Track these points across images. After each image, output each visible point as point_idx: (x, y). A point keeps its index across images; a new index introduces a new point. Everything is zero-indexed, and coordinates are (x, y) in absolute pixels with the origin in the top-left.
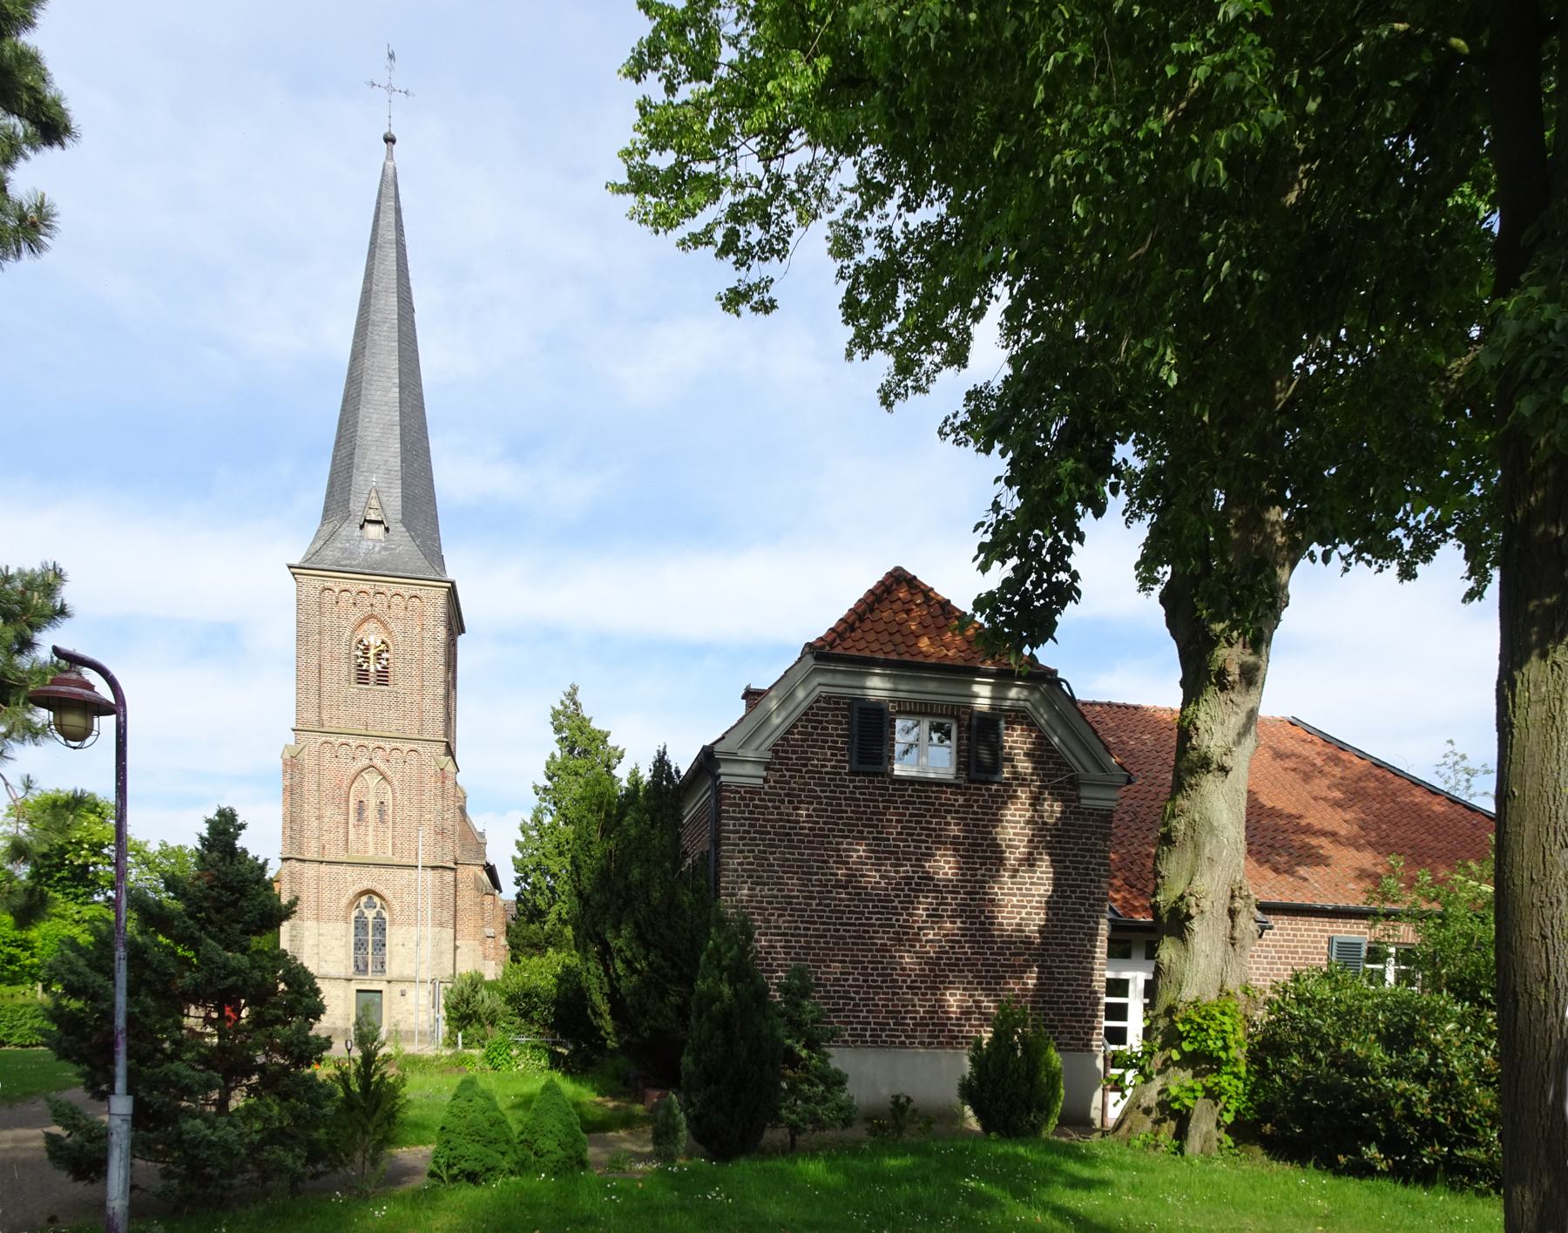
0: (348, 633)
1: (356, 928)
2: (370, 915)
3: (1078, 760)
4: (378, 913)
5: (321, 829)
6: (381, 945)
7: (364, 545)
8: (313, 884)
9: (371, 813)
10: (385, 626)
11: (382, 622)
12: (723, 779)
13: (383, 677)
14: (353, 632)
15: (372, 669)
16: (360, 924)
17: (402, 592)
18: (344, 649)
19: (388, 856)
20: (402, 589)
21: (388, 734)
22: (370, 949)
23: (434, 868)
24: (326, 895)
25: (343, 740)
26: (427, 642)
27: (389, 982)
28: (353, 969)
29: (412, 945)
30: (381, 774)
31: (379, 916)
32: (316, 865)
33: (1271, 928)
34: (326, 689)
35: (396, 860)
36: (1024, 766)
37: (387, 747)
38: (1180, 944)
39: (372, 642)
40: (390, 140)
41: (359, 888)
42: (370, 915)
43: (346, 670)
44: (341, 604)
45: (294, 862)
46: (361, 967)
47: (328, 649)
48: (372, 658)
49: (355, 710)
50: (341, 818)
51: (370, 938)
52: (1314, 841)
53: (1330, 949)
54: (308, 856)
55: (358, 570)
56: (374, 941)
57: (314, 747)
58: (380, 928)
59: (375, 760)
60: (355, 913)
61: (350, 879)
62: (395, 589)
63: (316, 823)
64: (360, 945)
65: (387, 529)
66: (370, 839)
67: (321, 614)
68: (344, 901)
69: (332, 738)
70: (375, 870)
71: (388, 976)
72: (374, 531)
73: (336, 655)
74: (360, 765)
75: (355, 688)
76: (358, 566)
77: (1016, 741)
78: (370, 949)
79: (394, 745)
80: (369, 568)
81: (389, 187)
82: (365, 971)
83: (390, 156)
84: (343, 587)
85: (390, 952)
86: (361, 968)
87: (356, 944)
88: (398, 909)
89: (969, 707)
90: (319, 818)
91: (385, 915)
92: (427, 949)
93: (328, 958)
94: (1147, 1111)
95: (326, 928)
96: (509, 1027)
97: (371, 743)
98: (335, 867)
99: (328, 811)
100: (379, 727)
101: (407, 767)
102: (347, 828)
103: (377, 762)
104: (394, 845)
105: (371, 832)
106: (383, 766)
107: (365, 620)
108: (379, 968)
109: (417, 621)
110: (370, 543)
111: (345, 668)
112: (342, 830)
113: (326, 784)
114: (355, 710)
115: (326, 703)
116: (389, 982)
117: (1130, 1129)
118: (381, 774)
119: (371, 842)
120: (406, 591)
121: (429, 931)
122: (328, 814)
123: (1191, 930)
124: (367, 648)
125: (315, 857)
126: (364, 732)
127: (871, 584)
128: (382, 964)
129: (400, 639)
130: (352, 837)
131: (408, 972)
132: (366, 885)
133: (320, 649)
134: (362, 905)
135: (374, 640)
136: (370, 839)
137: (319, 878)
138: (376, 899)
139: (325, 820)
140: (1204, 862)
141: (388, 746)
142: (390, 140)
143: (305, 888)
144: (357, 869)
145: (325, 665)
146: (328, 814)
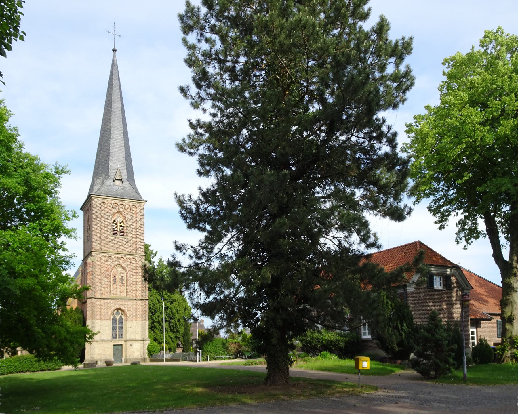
0: (110, 217)
1: (113, 322)
2: (118, 317)
3: (463, 284)
4: (121, 316)
5: (101, 287)
6: (121, 328)
7: (115, 187)
8: (99, 307)
9: (118, 281)
10: (123, 215)
11: (122, 214)
12: (408, 291)
13: (122, 233)
14: (112, 217)
15: (119, 230)
16: (114, 321)
17: (129, 204)
18: (109, 223)
19: (124, 295)
20: (129, 203)
21: (125, 253)
22: (118, 330)
23: (142, 300)
24: (103, 310)
25: (109, 255)
26: (138, 221)
27: (125, 341)
28: (111, 337)
29: (134, 327)
30: (122, 267)
31: (121, 317)
32: (100, 300)
33: (493, 319)
34: (103, 237)
35: (128, 297)
36: (455, 284)
37: (119, 257)
38: (510, 325)
39: (119, 221)
40: (114, 51)
41: (115, 307)
42: (118, 317)
43: (110, 231)
44: (108, 208)
45: (93, 299)
46: (114, 336)
47: (104, 223)
48: (119, 226)
49: (113, 244)
50: (108, 283)
51: (118, 326)
52: (482, 297)
53: (497, 322)
54: (97, 297)
55: (115, 196)
56: (119, 327)
57: (99, 258)
58: (121, 322)
59: (120, 262)
60: (112, 317)
61: (112, 305)
62: (127, 203)
63: (100, 285)
64: (114, 328)
65: (123, 182)
66: (118, 290)
67: (101, 211)
68: (110, 313)
69: (105, 255)
70: (120, 301)
71: (124, 339)
72: (118, 183)
73: (106, 225)
74: (115, 264)
75: (113, 237)
76: (114, 194)
77: (453, 279)
78: (118, 330)
79: (121, 256)
80: (118, 195)
81: (114, 64)
82: (116, 338)
83: (114, 56)
84: (109, 202)
85: (126, 331)
86: (114, 337)
87: (112, 328)
88: (129, 315)
89: (446, 273)
90: (101, 283)
91: (123, 317)
92: (139, 329)
93: (104, 334)
94: (509, 357)
95: (103, 322)
96: (223, 353)
97: (119, 256)
98: (106, 301)
99: (104, 280)
100: (121, 250)
101: (132, 264)
102: (110, 286)
103: (121, 263)
104: (127, 292)
105: (118, 288)
106: (123, 264)
107: (116, 213)
108: (121, 336)
109: (134, 214)
110: (117, 187)
111: (109, 230)
112: (109, 287)
113: (103, 271)
114: (113, 244)
115: (103, 242)
116: (125, 341)
117: (506, 361)
118: (122, 267)
119: (119, 291)
120: (131, 204)
121: (139, 322)
122: (104, 281)
123: (513, 322)
124: (117, 223)
125: (100, 297)
126: (117, 252)
127: (437, 252)
128: (122, 335)
129: (128, 220)
130: (112, 289)
131: (133, 337)
132: (118, 306)
133: (101, 223)
134: (115, 314)
135: (119, 220)
136: (118, 290)
137: (101, 305)
138: (120, 311)
139: (103, 284)
140: (514, 309)
141: (125, 257)
142: (114, 51)
143: (96, 308)
144: (114, 301)
145: (103, 229)
146: (104, 281)
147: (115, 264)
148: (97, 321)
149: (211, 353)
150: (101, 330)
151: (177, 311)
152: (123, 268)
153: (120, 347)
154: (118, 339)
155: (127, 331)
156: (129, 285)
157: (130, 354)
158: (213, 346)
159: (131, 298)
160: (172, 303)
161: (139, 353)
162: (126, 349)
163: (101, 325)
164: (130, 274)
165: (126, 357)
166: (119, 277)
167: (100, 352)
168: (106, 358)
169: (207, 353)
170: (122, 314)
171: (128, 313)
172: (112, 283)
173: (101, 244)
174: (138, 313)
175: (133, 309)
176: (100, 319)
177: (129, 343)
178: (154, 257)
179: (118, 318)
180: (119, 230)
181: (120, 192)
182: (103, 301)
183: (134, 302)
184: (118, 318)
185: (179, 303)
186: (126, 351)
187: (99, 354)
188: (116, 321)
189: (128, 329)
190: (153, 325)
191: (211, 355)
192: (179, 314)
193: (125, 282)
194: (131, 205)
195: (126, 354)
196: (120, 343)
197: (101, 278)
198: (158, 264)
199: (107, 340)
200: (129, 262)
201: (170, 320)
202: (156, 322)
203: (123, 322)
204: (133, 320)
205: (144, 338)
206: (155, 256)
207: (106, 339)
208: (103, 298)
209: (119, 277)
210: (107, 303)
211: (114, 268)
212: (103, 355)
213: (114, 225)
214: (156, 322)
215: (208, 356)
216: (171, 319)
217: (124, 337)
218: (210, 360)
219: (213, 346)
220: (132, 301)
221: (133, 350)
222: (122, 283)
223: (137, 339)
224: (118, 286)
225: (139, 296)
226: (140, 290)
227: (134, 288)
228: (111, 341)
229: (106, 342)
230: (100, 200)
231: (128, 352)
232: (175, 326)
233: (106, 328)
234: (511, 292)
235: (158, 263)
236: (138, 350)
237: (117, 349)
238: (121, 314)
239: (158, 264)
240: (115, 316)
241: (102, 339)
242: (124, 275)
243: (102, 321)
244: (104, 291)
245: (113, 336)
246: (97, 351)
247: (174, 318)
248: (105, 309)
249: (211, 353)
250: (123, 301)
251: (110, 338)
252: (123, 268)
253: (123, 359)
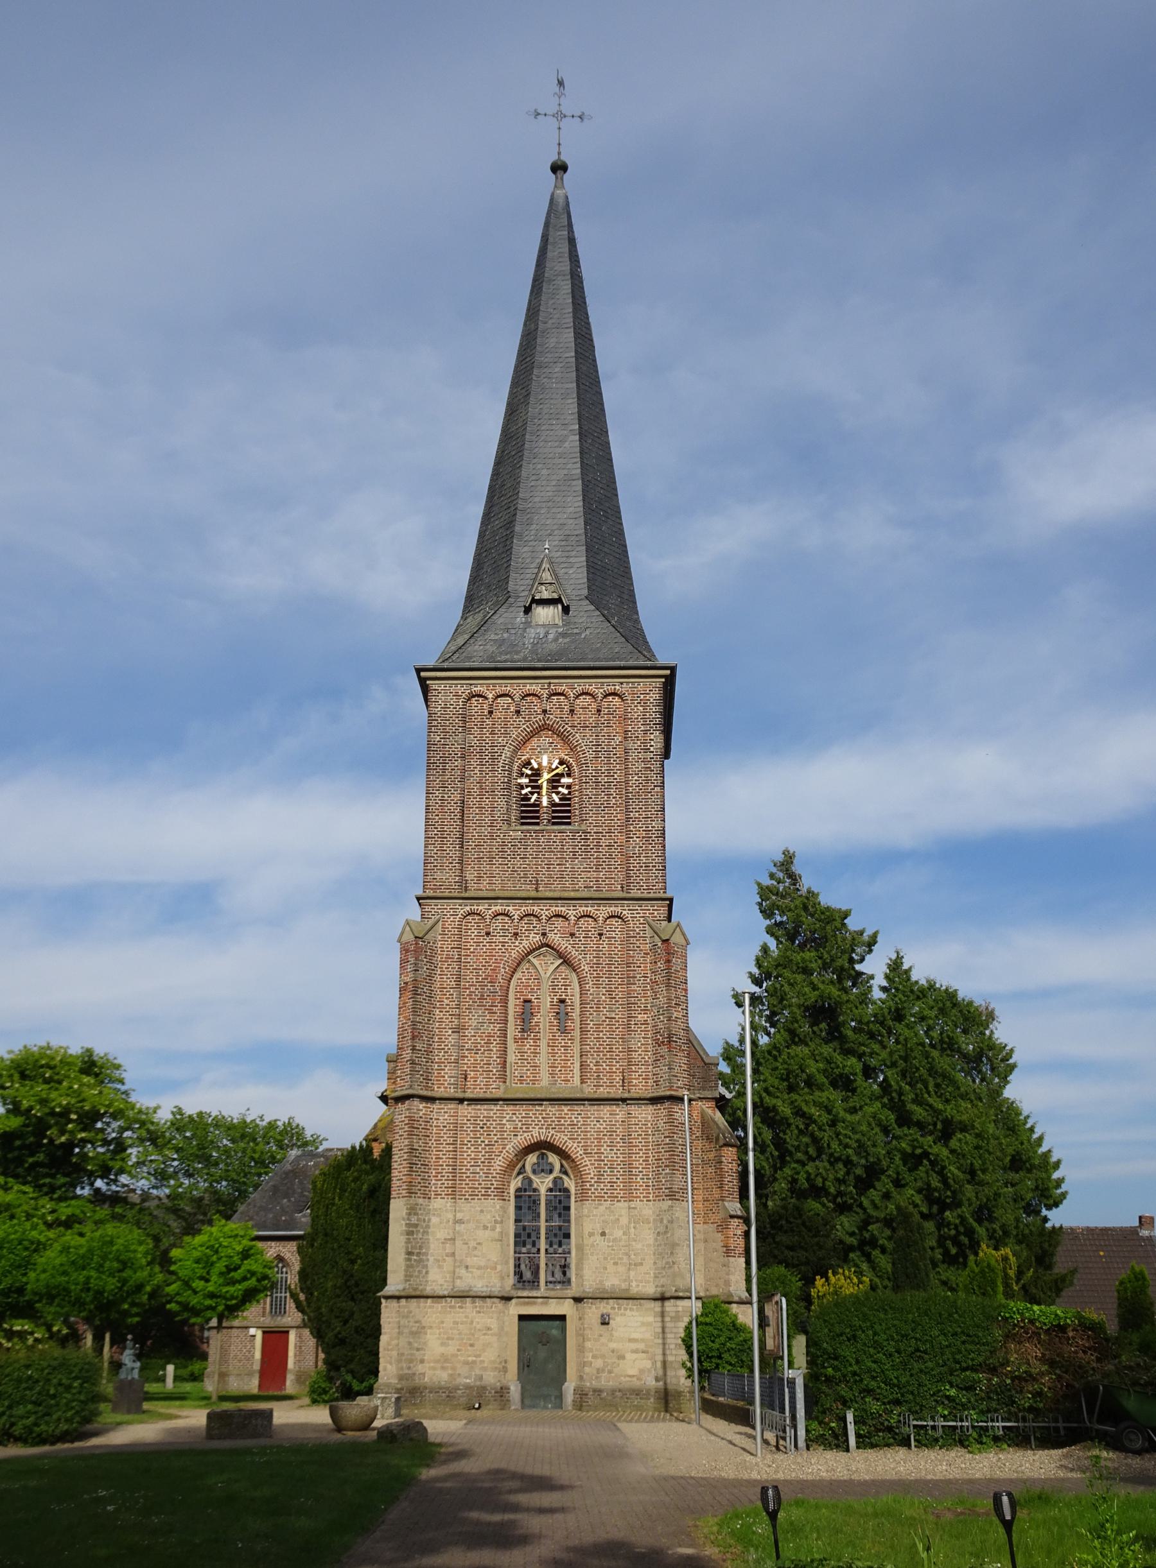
0: (507, 753)
1: (518, 1208)
2: (543, 1184)
6: (561, 1236)
8: (447, 1138)
9: (544, 1018)
10: (564, 738)
11: (560, 735)
13: (562, 813)
15: (545, 801)
16: (526, 1201)
18: (500, 776)
19: (573, 1084)
20: (592, 686)
22: (543, 1244)
23: (654, 1100)
26: (633, 756)
27: (578, 1300)
28: (511, 1280)
30: (560, 955)
31: (558, 1187)
32: (452, 1105)
34: (472, 833)
35: (588, 1091)
39: (545, 763)
41: (524, 1140)
42: (543, 1184)
44: (497, 714)
45: (416, 1102)
46: (528, 1275)
49: (518, 862)
51: (543, 1224)
54: (439, 1092)
56: (549, 1230)
57: (452, 922)
58: (560, 1205)
60: (515, 1183)
62: (580, 686)
63: (452, 1039)
64: (524, 1237)
66: (543, 1059)
68: (499, 1163)
70: (552, 1110)
71: (574, 1290)
75: (517, 833)
76: (525, 659)
78: (543, 1244)
82: (534, 1283)
84: (499, 690)
85: (580, 1248)
86: (526, 1277)
87: (517, 1236)
90: (458, 1030)
91: (570, 1183)
93: (469, 1261)
95: (467, 1209)
97: (544, 910)
98: (483, 1110)
99: (473, 1020)
103: (555, 938)
106: (564, 944)
107: (535, 733)
108: (558, 1275)
109: (616, 728)
112: (495, 1047)
113: (470, 977)
114: (518, 862)
115: (471, 855)
116: (578, 1300)
118: (560, 955)
124: (537, 773)
125: (451, 1092)
126: (533, 894)
128: (565, 1268)
130: (511, 1058)
131: (612, 1281)
132: (537, 1134)
133: (463, 779)
134: (528, 1168)
135: (547, 760)
136: (543, 1059)
137: (456, 1127)
138: (553, 1159)
143: (432, 1143)
144: (522, 1110)
145: (470, 801)
147: (525, 944)
148: (437, 1204)
149: (869, 1391)
150: (458, 1243)
151: (972, 1172)
152: (566, 961)
153: (553, 1330)
154: (543, 1290)
155: (587, 1250)
156: (591, 1040)
157: (599, 1363)
158: (877, 1346)
159: (603, 1092)
160: (945, 1135)
161: (648, 1364)
162: (581, 1334)
163: (461, 1222)
164: (597, 986)
165: (581, 1378)
166: (545, 1002)
167: (451, 1349)
168: (481, 1378)
169: (843, 1390)
170: (566, 1173)
171: (589, 1167)
172: (512, 1031)
173: (461, 862)
174: (638, 1163)
175: (611, 1146)
176: (454, 1193)
177: (593, 1311)
178: (868, 957)
179: (543, 1191)
180: (545, 801)
181: (553, 646)
182: (465, 1110)
183: (620, 1111)
184: (543, 1191)
185: (978, 1136)
186: (581, 1349)
187: (445, 1359)
188: (536, 1202)
189: (588, 1241)
190: (867, 1235)
191: (875, 1407)
192: (981, 1183)
193: (575, 1025)
194: (599, 693)
195: (583, 1365)
196: (552, 1309)
197: (458, 1007)
198: (885, 983)
199: (485, 1291)
200: (593, 934)
201: (942, 1211)
202: (878, 1220)
203: (568, 1208)
204: (613, 1198)
205: (663, 1294)
206: (870, 951)
207: (480, 1286)
208: (469, 1095)
209: (545, 1002)
210: (488, 1118)
211: (525, 966)
212: (466, 1363)
213: (525, 781)
214: (878, 1220)
215: (850, 1417)
216: (944, 1207)
217: (573, 1279)
218: (864, 1442)
219: (877, 1346)
220: (605, 1110)
221: (613, 1345)
222: (564, 1031)
223: (635, 1289)
224: (543, 1043)
225: (641, 1087)
226: (649, 1057)
227: (618, 1048)
228: (508, 1299)
229: (478, 1302)
230: (462, 689)
231: (589, 1357)
232: (965, 1240)
233: (482, 1235)
234: (1099, 1442)
235: (887, 977)
236: (641, 1346)
237: (544, 1339)
238: (557, 1167)
239: (885, 983)
240: (530, 1181)
241: (461, 1285)
242: (574, 994)
243: (461, 1203)
244: (475, 1065)
245: (519, 1274)
246: (434, 1345)
247: (959, 1205)
248: (476, 1146)
249: (869, 1391)
250: (565, 1109)
251: (501, 1278)
252: (566, 961)
253: (569, 1387)
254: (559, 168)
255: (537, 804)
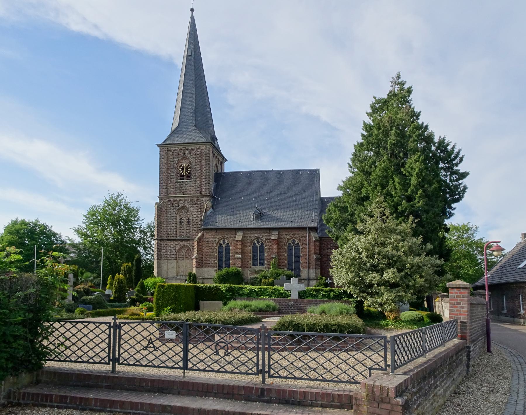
9: (185, 223)
13: (189, 177)
254: (192, 10)
255: (183, 175)
